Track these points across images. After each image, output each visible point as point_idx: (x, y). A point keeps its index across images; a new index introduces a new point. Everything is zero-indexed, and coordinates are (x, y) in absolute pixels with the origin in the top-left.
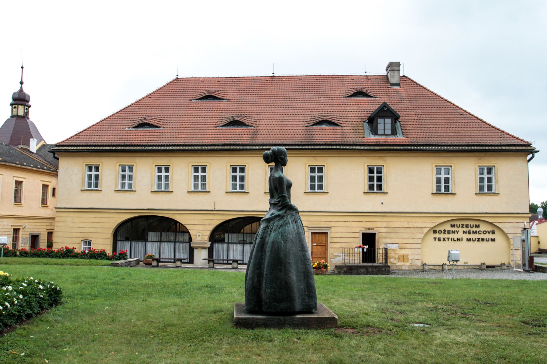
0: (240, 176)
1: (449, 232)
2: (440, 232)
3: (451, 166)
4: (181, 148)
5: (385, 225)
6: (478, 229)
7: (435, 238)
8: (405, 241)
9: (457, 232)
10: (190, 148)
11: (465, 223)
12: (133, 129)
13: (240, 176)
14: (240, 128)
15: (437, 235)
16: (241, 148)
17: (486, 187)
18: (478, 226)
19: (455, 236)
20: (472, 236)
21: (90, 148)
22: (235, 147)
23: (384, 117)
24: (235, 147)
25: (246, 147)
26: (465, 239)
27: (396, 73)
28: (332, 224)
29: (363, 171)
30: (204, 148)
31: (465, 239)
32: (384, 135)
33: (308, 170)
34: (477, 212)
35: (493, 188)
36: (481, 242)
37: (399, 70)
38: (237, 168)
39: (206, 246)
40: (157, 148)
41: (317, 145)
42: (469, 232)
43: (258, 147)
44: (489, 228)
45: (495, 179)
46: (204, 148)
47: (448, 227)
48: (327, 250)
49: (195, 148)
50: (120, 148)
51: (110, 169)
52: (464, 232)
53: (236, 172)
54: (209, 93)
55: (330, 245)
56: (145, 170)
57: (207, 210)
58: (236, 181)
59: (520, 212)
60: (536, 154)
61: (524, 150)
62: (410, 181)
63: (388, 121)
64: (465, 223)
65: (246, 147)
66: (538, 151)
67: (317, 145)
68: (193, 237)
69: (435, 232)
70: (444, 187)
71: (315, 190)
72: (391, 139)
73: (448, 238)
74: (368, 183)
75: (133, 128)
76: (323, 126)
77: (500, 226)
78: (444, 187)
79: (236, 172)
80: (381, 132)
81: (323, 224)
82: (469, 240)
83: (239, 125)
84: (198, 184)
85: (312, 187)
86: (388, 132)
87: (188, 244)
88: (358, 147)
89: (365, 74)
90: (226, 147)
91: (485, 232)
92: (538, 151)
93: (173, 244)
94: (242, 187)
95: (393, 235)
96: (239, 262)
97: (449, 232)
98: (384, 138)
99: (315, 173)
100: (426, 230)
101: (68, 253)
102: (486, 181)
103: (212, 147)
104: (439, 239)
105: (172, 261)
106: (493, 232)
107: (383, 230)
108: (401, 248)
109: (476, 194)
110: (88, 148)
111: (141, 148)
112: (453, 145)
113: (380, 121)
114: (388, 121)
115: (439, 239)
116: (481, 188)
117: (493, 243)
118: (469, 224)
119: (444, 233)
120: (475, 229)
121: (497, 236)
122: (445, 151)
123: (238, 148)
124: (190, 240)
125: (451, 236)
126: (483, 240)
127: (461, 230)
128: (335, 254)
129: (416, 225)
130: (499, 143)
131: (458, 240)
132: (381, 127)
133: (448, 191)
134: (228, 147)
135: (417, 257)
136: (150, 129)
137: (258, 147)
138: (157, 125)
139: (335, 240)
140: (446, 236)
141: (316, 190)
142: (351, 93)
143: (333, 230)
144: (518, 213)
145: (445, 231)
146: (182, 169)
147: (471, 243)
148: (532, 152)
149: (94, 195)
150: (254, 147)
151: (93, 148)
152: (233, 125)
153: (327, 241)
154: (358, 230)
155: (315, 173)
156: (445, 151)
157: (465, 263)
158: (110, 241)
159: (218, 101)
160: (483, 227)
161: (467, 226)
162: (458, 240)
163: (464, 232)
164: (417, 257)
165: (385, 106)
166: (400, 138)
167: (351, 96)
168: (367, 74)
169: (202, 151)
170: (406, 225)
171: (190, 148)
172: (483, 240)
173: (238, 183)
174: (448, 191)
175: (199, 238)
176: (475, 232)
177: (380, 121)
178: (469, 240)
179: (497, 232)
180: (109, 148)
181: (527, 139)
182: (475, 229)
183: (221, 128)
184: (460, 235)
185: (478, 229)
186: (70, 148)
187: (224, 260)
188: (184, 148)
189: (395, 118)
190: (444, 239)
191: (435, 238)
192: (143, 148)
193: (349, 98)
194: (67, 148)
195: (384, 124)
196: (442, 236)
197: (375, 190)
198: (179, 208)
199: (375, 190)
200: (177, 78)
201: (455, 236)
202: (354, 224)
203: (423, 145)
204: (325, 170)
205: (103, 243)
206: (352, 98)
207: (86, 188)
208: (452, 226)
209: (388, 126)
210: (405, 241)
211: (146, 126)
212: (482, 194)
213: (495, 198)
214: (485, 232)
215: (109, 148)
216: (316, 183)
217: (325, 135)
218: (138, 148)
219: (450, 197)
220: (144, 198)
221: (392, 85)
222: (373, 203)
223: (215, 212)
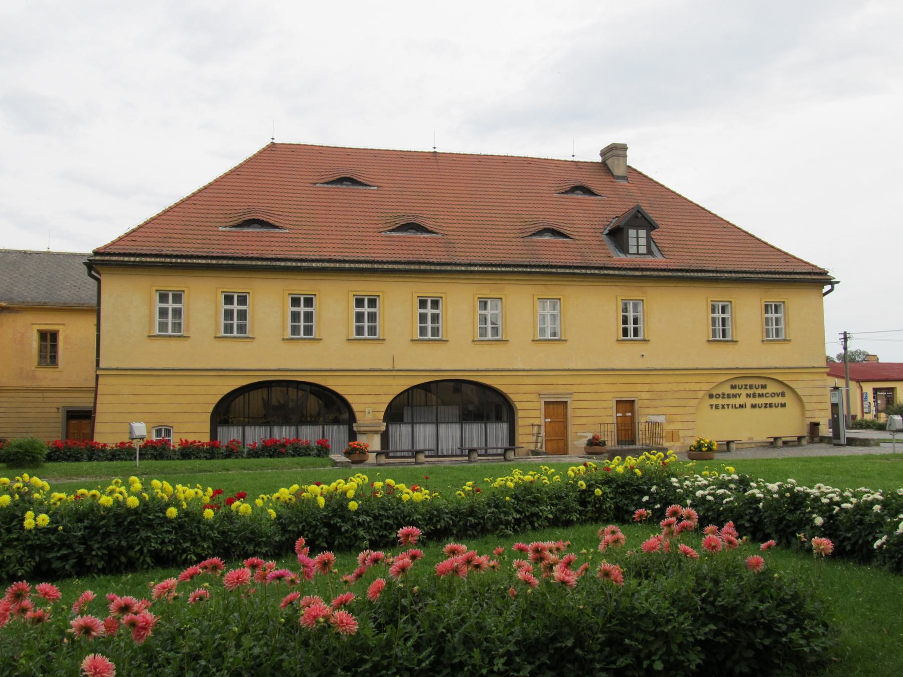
0: (305, 312)
1: (729, 396)
2: (718, 396)
3: (731, 302)
4: (338, 265)
5: (647, 388)
6: (764, 391)
7: (711, 406)
8: (674, 410)
9: (739, 396)
10: (352, 265)
11: (749, 382)
12: (234, 229)
13: (238, 311)
14: (419, 235)
15: (714, 401)
16: (438, 268)
17: (774, 333)
18: (764, 387)
19: (737, 401)
20: (758, 401)
21: (168, 260)
22: (428, 267)
23: (638, 227)
24: (428, 267)
25: (444, 268)
26: (748, 405)
27: (621, 159)
28: (574, 389)
29: (615, 308)
30: (376, 266)
31: (748, 405)
32: (638, 254)
33: (417, 304)
34: (764, 366)
35: (641, 332)
36: (768, 409)
37: (625, 156)
38: (363, 300)
39: (378, 429)
40: (294, 264)
41: (552, 267)
42: (754, 396)
43: (463, 268)
44: (778, 389)
45: (785, 319)
46: (376, 266)
47: (727, 390)
48: (566, 428)
49: (361, 266)
50: (225, 262)
51: (203, 299)
52: (748, 396)
53: (232, 303)
54: (345, 173)
55: (571, 421)
56: (269, 301)
57: (381, 370)
58: (232, 319)
59: (816, 365)
60: (836, 285)
61: (817, 280)
62: (677, 321)
63: (643, 233)
64: (749, 382)
65: (444, 268)
66: (838, 282)
67: (552, 267)
68: (358, 416)
69: (711, 396)
70: (721, 333)
71: (167, 331)
72: (650, 261)
73: (728, 405)
74: (419, 325)
75: (234, 226)
76: (547, 238)
77: (793, 385)
78: (721, 333)
79: (232, 303)
80: (632, 250)
81: (561, 389)
82: (753, 406)
83: (418, 231)
84: (363, 327)
85: (228, 328)
86: (643, 250)
87: (346, 427)
88: (611, 272)
89: (571, 159)
90: (412, 267)
91: (773, 395)
92: (838, 282)
93: (321, 427)
94: (435, 332)
95: (658, 403)
96: (479, 452)
97: (729, 396)
98: (638, 258)
99: (299, 306)
100: (700, 394)
101: (122, 453)
102: (548, 318)
103: (390, 266)
104: (717, 407)
105: (410, 454)
106: (783, 394)
107: (644, 396)
108: (669, 422)
109: (763, 341)
110: (163, 260)
111: (265, 263)
112: (681, 271)
113: (632, 233)
114: (643, 233)
115: (717, 407)
116: (625, 332)
117: (783, 409)
118: (754, 385)
119: (723, 398)
120: (760, 391)
121: (788, 399)
122: (350, 270)
123: (433, 268)
124: (352, 418)
125: (732, 401)
126: (771, 405)
127: (744, 392)
128: (579, 434)
129: (687, 387)
130: (791, 270)
131: (741, 406)
132: (632, 241)
133: (311, 334)
134: (417, 267)
135: (690, 433)
136: (262, 230)
137: (463, 268)
138: (276, 224)
139: (579, 412)
140: (725, 401)
141: (170, 333)
142: (567, 188)
143: (576, 397)
144: (814, 367)
145: (723, 394)
146: (335, 302)
147: (757, 410)
148: (831, 282)
149: (175, 345)
150: (458, 268)
151: (174, 260)
152: (406, 231)
153: (565, 415)
154: (609, 396)
155: (299, 306)
156: (350, 270)
157: (750, 439)
158: (207, 427)
159: (361, 187)
160: (772, 388)
161: (751, 387)
162: (741, 406)
163: (748, 396)
164: (690, 433)
165: (638, 211)
166: (659, 260)
167: (566, 192)
168: (575, 159)
169: (795, 281)
170: (675, 387)
171: (352, 265)
172: (771, 405)
173: (170, 320)
174: (375, 335)
175: (369, 416)
176: (761, 396)
177: (632, 233)
178: (753, 406)
179: (788, 393)
180: (204, 261)
181: (821, 264)
182: (760, 391)
183: (388, 233)
184: (743, 400)
185: (764, 391)
186: (126, 259)
187: (497, 448)
188: (342, 265)
189: (651, 226)
190: (723, 407)
191: (711, 406)
192: (269, 263)
193: (565, 196)
194: (121, 258)
195: (637, 238)
196: (720, 402)
197: (235, 334)
198: (334, 367)
199: (235, 334)
200: (273, 144)
201: (737, 401)
202: (605, 388)
203: (697, 271)
204: (249, 300)
205: (195, 429)
206: (570, 196)
207: (157, 332)
208: (733, 387)
209: (643, 242)
210: (674, 410)
211: (256, 225)
212: (423, 340)
213: (786, 346)
214: (773, 395)
215: (204, 261)
216: (302, 324)
217: (551, 251)
218: (259, 263)
219: (730, 347)
220: (269, 350)
221: (618, 178)
222: (628, 356)
223: (394, 373)
